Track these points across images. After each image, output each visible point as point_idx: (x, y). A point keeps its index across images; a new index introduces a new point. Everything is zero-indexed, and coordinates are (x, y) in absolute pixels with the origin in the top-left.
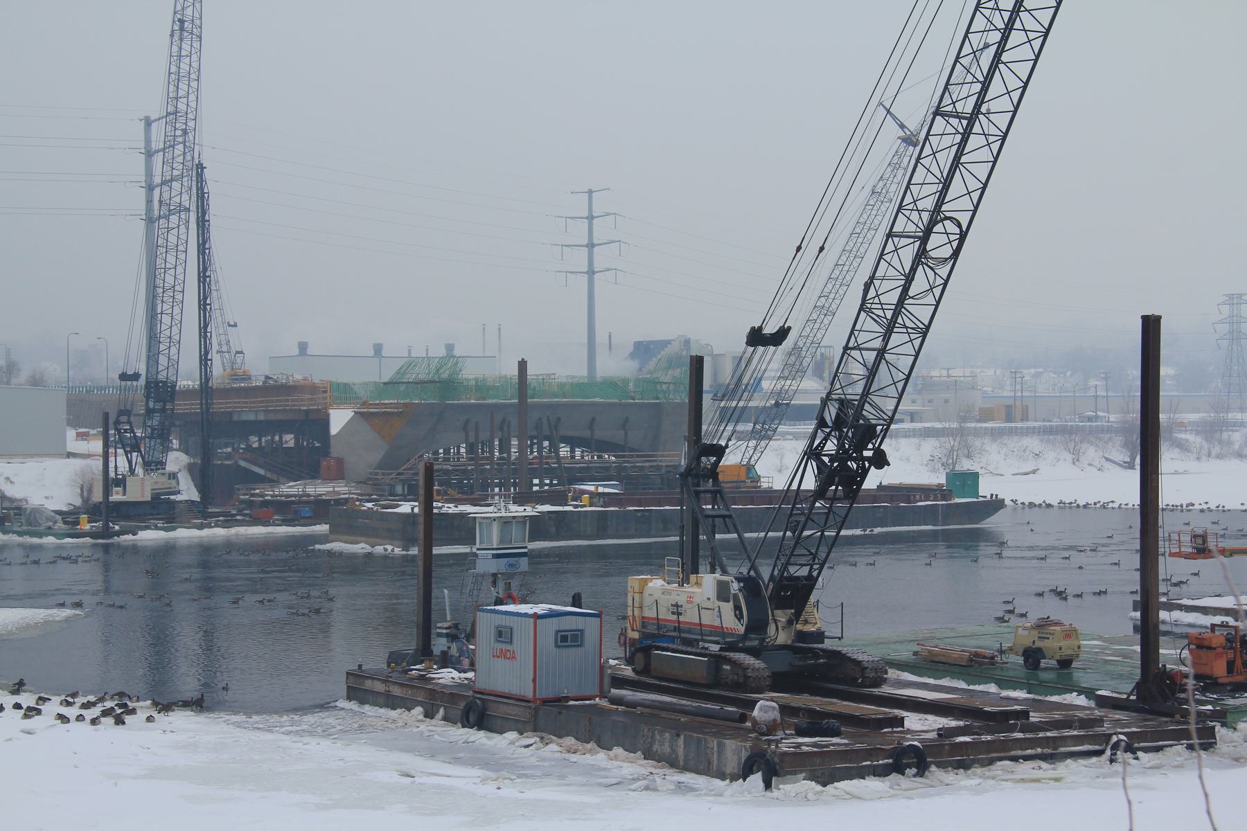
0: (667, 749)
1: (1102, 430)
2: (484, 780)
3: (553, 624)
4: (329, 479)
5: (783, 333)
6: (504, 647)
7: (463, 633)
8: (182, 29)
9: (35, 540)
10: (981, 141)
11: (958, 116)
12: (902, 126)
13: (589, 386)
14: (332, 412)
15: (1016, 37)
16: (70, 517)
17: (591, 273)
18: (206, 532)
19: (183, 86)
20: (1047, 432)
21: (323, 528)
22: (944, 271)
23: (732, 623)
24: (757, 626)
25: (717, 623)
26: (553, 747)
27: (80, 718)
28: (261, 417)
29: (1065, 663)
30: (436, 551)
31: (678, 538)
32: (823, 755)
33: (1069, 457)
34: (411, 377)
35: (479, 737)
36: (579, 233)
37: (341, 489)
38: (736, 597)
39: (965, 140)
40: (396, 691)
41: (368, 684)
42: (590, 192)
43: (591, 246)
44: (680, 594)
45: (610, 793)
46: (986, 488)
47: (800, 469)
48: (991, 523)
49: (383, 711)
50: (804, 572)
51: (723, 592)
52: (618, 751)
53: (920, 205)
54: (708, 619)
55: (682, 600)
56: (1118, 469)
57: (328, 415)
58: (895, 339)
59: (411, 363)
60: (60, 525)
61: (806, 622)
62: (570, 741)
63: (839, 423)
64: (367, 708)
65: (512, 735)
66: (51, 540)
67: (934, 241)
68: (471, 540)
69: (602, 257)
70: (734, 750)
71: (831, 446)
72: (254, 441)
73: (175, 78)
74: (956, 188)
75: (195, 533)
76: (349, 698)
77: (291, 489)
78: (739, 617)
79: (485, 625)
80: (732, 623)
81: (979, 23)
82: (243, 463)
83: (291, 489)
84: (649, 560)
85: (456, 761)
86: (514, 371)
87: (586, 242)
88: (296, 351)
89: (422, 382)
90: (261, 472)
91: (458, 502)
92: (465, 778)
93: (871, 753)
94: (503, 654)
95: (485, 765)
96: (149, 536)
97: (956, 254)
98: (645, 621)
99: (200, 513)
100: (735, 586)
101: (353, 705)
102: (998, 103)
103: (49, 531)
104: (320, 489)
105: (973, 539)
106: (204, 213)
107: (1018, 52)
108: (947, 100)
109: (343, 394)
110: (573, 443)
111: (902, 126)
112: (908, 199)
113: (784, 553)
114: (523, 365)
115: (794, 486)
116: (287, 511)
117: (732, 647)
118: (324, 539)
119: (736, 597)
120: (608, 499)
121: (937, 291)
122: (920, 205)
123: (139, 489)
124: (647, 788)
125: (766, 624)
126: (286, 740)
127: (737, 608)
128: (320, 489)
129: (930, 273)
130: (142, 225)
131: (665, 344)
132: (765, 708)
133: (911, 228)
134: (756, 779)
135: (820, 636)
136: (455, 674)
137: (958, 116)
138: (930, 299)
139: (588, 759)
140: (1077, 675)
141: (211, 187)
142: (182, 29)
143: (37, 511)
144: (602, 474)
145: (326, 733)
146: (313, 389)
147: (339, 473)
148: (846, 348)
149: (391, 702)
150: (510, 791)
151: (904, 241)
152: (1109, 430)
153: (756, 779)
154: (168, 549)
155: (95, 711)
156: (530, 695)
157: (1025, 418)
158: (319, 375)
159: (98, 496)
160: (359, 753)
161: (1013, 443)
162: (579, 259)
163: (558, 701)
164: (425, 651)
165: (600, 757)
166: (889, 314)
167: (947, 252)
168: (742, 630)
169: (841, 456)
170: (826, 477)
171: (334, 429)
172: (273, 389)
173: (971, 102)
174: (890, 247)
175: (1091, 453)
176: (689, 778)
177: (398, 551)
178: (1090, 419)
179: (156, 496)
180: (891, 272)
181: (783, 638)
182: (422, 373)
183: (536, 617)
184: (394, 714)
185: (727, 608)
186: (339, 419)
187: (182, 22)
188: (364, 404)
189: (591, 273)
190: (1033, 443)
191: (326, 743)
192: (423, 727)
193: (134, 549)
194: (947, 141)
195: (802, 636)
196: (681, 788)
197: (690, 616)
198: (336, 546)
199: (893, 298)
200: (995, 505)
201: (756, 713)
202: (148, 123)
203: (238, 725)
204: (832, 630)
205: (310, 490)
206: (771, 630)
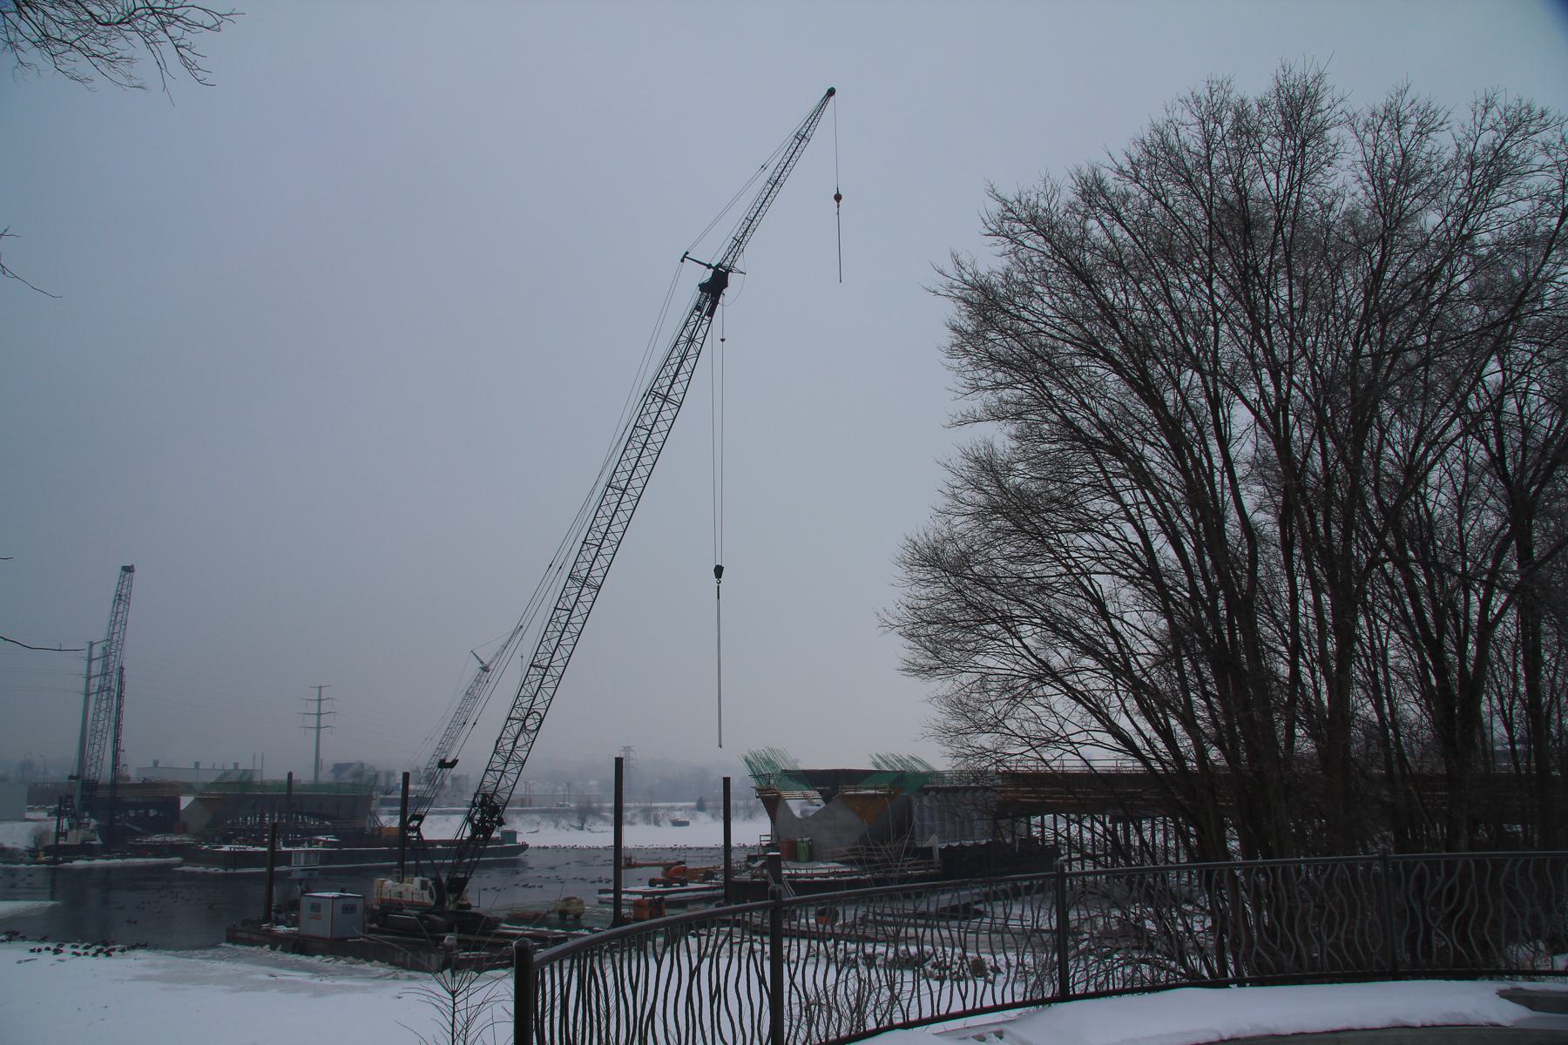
0: (401, 960)
1: (568, 811)
2: (312, 978)
3: (341, 902)
4: (177, 833)
5: (455, 762)
6: (316, 913)
7: (295, 905)
8: (120, 599)
9: (14, 866)
10: (550, 678)
11: (541, 667)
12: (482, 662)
13: (316, 786)
14: (182, 798)
15: (566, 635)
16: (33, 853)
17: (318, 728)
18: (111, 861)
19: (117, 628)
20: (542, 812)
21: (177, 859)
22: (533, 736)
23: (427, 899)
24: (440, 901)
25: (421, 900)
26: (342, 962)
27: (86, 954)
28: (140, 800)
29: (577, 917)
30: (276, 869)
31: (276, 869)
32: (480, 960)
33: (553, 824)
34: (225, 780)
35: (303, 958)
36: (314, 708)
37: (186, 839)
38: (430, 888)
39: (544, 676)
40: (255, 937)
41: (239, 934)
42: (320, 687)
43: (319, 714)
44: (401, 887)
45: (376, 981)
46: (520, 840)
47: (463, 827)
48: (521, 856)
49: (247, 948)
50: (463, 876)
51: (424, 885)
52: (376, 962)
53: (523, 705)
54: (416, 899)
55: (402, 889)
56: (576, 831)
57: (179, 799)
58: (509, 766)
59: (226, 773)
60: (28, 858)
61: (463, 899)
62: (351, 959)
63: (482, 804)
64: (238, 946)
65: (319, 957)
66: (23, 865)
67: (528, 722)
68: (288, 863)
69: (325, 721)
70: (436, 959)
71: (478, 816)
72: (132, 813)
73: (113, 623)
74: (539, 699)
75: (119, 861)
76: (228, 942)
77: (158, 838)
78: (432, 897)
79: (305, 903)
80: (427, 899)
81: (551, 628)
82: (127, 825)
83: (158, 838)
84: (387, 872)
85: (293, 969)
86: (285, 778)
87: (316, 712)
88: (152, 765)
89: (232, 783)
90: (138, 829)
91: (254, 846)
92: (301, 977)
93: (500, 958)
94: (315, 917)
95: (309, 970)
96: (79, 863)
97: (538, 728)
98: (383, 901)
99: (107, 850)
100: (430, 883)
101: (230, 945)
102: (558, 663)
103: (21, 861)
104: (175, 839)
105: (515, 863)
106: (121, 692)
107: (567, 640)
108: (536, 660)
109: (188, 788)
110: (310, 815)
111: (482, 662)
112: (518, 703)
113: (454, 868)
114: (290, 775)
115: (459, 838)
116: (157, 850)
117: (428, 912)
118: (180, 865)
119: (430, 888)
120: (332, 844)
121: (529, 745)
122: (523, 705)
123: (74, 838)
124: (394, 978)
125: (444, 901)
126: (202, 962)
127: (431, 893)
128: (175, 839)
129: (526, 737)
130: (83, 697)
131: (350, 765)
132: (449, 939)
133: (518, 716)
134: (447, 972)
135: (469, 906)
136: (285, 928)
137: (541, 667)
138: (526, 748)
139: (361, 967)
140: (583, 922)
141: (127, 679)
142: (120, 599)
143: (14, 850)
144: (325, 832)
145: (221, 958)
146: (170, 785)
147: (184, 830)
148: (487, 770)
149: (251, 943)
150: (327, 982)
151: (515, 722)
152: (571, 811)
153: (447, 972)
154: (89, 870)
155: (92, 951)
156: (329, 936)
157: (530, 805)
158: (169, 777)
159: (51, 841)
160: (241, 967)
161: (527, 817)
162: (313, 721)
163: (343, 939)
164: (267, 919)
165: (367, 966)
166: (508, 755)
167: (534, 727)
168: (433, 903)
169: (482, 820)
170: (475, 830)
171: (183, 807)
172: (146, 785)
173: (547, 661)
174: (509, 724)
175: (564, 822)
176: (412, 973)
177: (221, 871)
178: (561, 806)
179: (83, 842)
180: (509, 736)
181: (452, 908)
182: (233, 778)
183: (333, 898)
184: (254, 949)
185: (426, 893)
186: (185, 801)
187: (120, 595)
188: (201, 794)
189: (318, 728)
190: (536, 817)
191: (223, 963)
192: (271, 954)
193: (70, 870)
194: (535, 678)
195: (461, 907)
196: (410, 978)
197: (407, 897)
198: (186, 868)
199: (510, 747)
200: (525, 847)
201: (445, 941)
202: (92, 644)
203: (173, 955)
204: (474, 903)
205: (168, 839)
206: (447, 904)
